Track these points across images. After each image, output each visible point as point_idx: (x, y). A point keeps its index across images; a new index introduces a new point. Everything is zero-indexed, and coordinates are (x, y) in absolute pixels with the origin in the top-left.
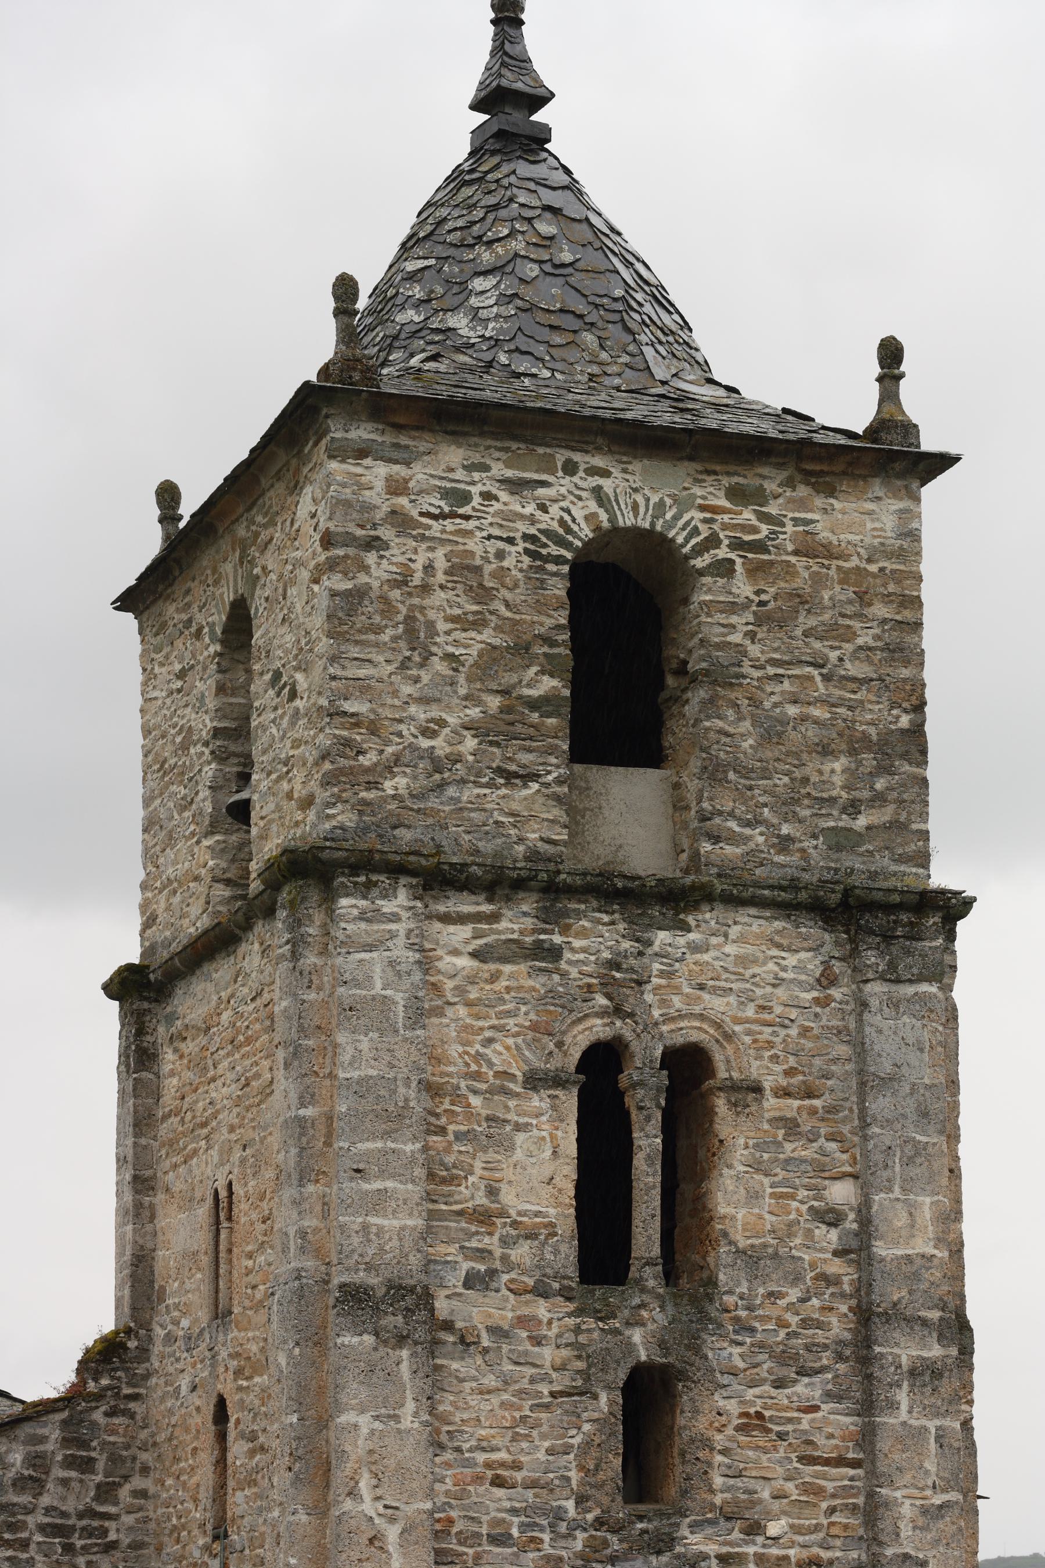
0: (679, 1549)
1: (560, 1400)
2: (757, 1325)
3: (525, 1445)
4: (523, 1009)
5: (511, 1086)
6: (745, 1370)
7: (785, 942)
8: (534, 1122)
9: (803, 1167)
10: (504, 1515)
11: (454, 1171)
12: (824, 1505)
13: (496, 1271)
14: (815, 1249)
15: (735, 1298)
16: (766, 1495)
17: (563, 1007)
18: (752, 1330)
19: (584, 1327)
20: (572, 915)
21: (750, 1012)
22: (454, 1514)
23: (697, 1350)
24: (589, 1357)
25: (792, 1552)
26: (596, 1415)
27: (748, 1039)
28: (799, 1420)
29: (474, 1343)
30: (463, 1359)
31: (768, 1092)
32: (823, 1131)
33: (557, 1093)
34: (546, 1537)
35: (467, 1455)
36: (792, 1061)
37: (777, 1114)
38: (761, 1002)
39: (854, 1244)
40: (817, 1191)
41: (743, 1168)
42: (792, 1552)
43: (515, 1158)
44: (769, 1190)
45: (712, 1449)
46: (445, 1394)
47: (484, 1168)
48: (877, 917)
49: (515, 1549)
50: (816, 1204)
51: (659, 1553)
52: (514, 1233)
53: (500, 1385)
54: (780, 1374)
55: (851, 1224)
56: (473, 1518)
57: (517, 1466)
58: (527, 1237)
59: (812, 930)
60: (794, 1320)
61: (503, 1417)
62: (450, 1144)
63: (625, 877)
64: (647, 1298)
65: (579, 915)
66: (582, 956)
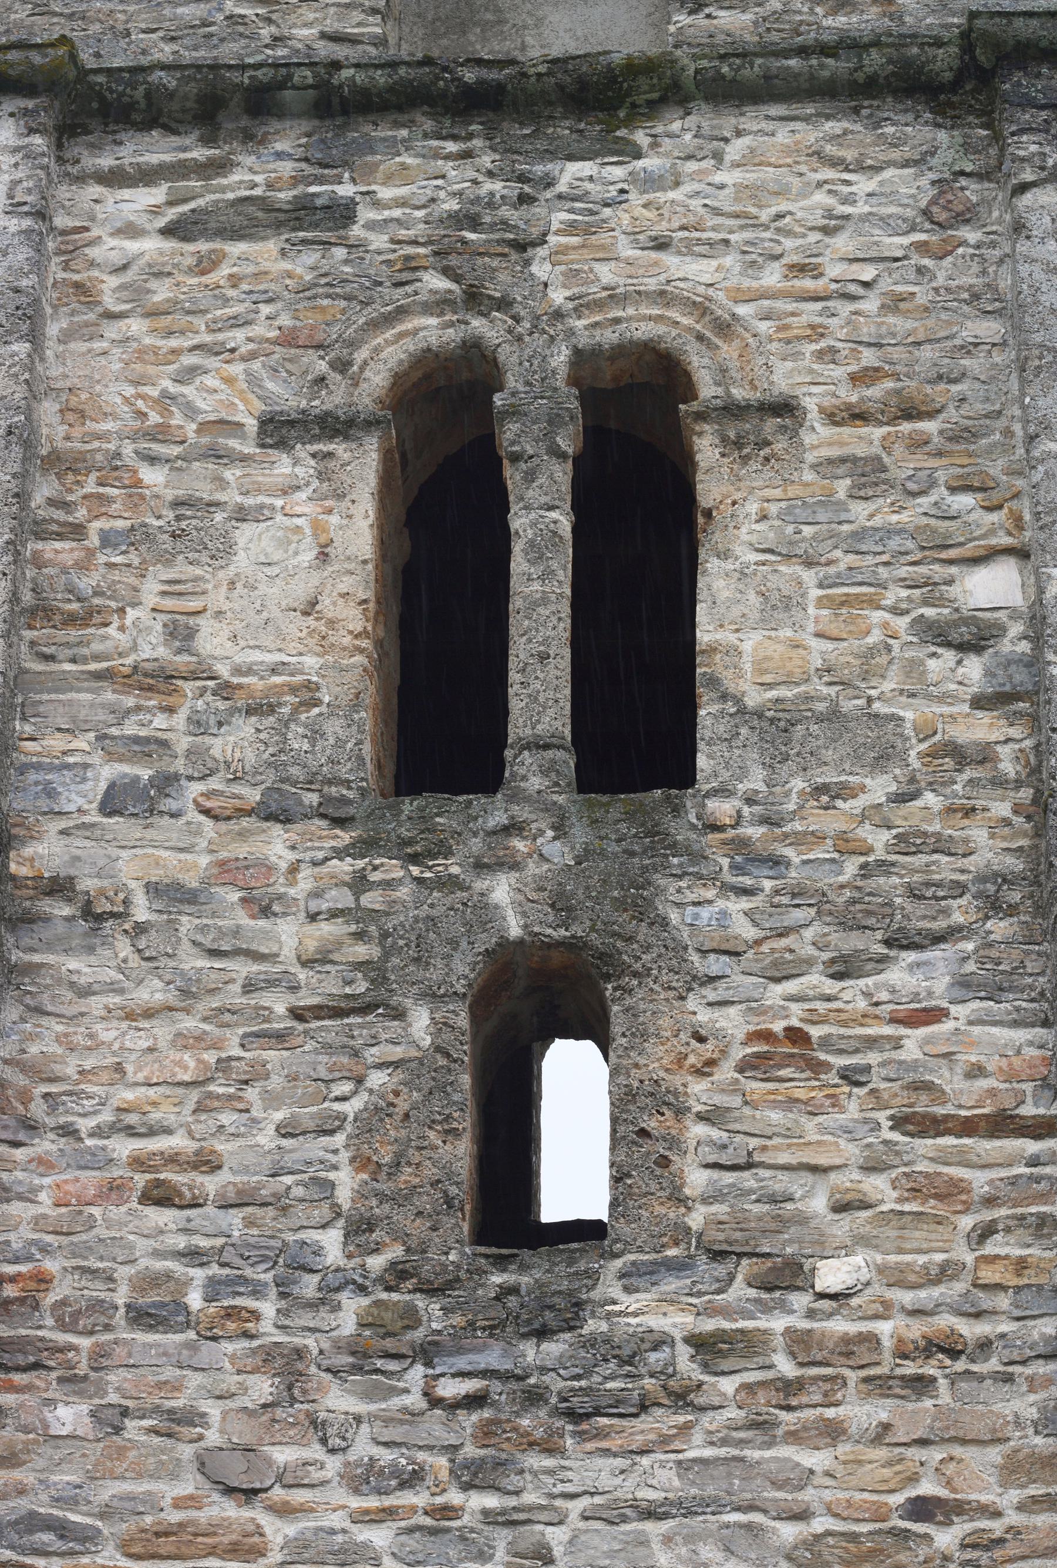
0: (593, 1326)
1: (315, 1024)
2: (789, 852)
3: (226, 1118)
4: (266, 310)
5: (233, 443)
6: (758, 942)
7: (850, 155)
8: (279, 503)
9: (894, 544)
10: (169, 1264)
11: (96, 601)
12: (967, 1222)
13: (176, 777)
14: (929, 697)
15: (737, 803)
16: (819, 1204)
17: (348, 298)
18: (777, 862)
19: (375, 877)
20: (380, 147)
21: (772, 277)
22: (52, 1265)
23: (642, 909)
24: (385, 935)
25: (884, 1328)
26: (397, 1052)
27: (764, 327)
28: (897, 1044)
29: (113, 915)
30: (91, 950)
31: (813, 415)
32: (941, 476)
33: (331, 447)
34: (268, 1308)
35: (89, 1142)
36: (869, 357)
37: (835, 452)
38: (795, 259)
39: (1021, 677)
40: (931, 590)
41: (754, 557)
42: (884, 1328)
43: (231, 571)
44: (815, 593)
45: (680, 1112)
46: (45, 1021)
47: (164, 593)
48: (1038, 75)
49: (192, 1335)
50: (930, 612)
51: (542, 1334)
52: (222, 705)
53: (171, 997)
54: (846, 948)
55: (1014, 643)
56: (94, 1272)
57: (206, 1163)
58: (250, 712)
59: (915, 131)
60: (880, 840)
61: (180, 1064)
62: (91, 553)
63: (480, 62)
64: (521, 811)
65: (393, 147)
66: (397, 213)
